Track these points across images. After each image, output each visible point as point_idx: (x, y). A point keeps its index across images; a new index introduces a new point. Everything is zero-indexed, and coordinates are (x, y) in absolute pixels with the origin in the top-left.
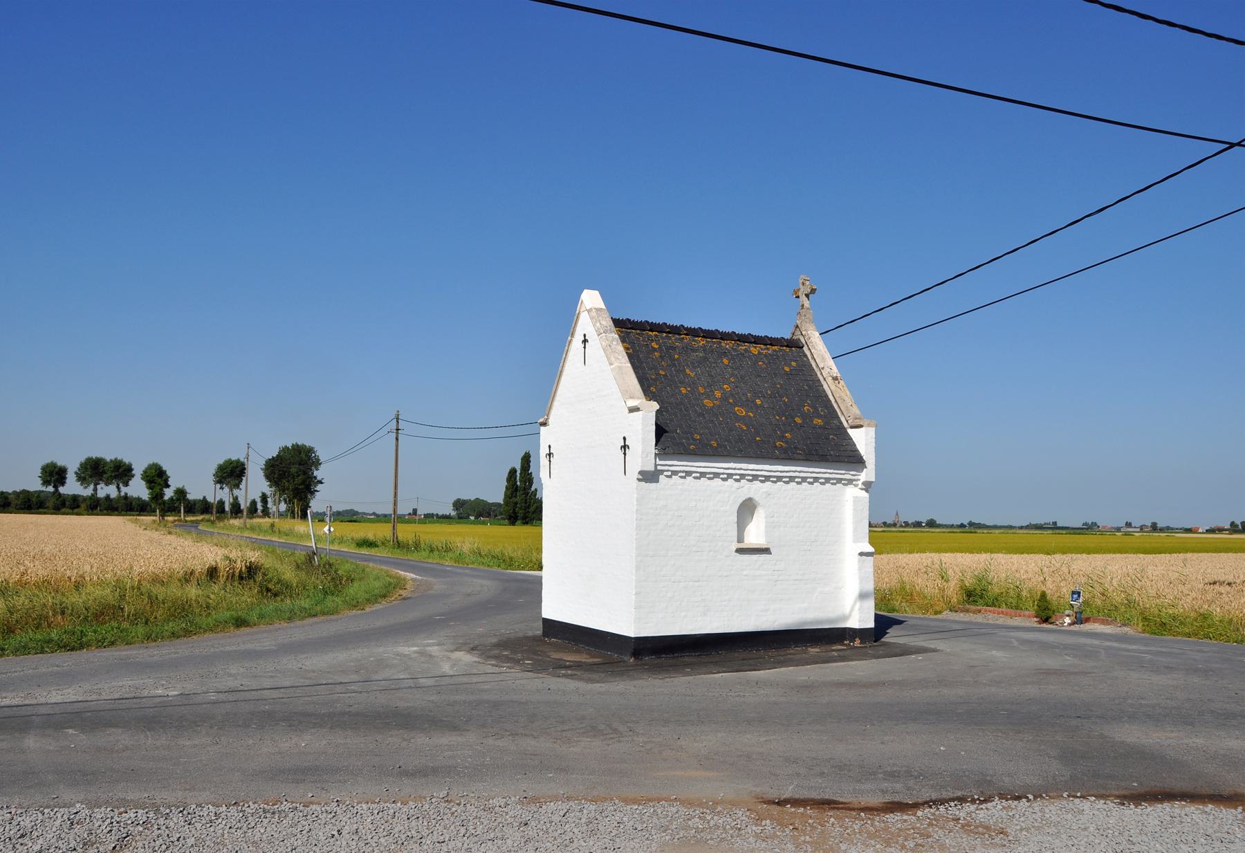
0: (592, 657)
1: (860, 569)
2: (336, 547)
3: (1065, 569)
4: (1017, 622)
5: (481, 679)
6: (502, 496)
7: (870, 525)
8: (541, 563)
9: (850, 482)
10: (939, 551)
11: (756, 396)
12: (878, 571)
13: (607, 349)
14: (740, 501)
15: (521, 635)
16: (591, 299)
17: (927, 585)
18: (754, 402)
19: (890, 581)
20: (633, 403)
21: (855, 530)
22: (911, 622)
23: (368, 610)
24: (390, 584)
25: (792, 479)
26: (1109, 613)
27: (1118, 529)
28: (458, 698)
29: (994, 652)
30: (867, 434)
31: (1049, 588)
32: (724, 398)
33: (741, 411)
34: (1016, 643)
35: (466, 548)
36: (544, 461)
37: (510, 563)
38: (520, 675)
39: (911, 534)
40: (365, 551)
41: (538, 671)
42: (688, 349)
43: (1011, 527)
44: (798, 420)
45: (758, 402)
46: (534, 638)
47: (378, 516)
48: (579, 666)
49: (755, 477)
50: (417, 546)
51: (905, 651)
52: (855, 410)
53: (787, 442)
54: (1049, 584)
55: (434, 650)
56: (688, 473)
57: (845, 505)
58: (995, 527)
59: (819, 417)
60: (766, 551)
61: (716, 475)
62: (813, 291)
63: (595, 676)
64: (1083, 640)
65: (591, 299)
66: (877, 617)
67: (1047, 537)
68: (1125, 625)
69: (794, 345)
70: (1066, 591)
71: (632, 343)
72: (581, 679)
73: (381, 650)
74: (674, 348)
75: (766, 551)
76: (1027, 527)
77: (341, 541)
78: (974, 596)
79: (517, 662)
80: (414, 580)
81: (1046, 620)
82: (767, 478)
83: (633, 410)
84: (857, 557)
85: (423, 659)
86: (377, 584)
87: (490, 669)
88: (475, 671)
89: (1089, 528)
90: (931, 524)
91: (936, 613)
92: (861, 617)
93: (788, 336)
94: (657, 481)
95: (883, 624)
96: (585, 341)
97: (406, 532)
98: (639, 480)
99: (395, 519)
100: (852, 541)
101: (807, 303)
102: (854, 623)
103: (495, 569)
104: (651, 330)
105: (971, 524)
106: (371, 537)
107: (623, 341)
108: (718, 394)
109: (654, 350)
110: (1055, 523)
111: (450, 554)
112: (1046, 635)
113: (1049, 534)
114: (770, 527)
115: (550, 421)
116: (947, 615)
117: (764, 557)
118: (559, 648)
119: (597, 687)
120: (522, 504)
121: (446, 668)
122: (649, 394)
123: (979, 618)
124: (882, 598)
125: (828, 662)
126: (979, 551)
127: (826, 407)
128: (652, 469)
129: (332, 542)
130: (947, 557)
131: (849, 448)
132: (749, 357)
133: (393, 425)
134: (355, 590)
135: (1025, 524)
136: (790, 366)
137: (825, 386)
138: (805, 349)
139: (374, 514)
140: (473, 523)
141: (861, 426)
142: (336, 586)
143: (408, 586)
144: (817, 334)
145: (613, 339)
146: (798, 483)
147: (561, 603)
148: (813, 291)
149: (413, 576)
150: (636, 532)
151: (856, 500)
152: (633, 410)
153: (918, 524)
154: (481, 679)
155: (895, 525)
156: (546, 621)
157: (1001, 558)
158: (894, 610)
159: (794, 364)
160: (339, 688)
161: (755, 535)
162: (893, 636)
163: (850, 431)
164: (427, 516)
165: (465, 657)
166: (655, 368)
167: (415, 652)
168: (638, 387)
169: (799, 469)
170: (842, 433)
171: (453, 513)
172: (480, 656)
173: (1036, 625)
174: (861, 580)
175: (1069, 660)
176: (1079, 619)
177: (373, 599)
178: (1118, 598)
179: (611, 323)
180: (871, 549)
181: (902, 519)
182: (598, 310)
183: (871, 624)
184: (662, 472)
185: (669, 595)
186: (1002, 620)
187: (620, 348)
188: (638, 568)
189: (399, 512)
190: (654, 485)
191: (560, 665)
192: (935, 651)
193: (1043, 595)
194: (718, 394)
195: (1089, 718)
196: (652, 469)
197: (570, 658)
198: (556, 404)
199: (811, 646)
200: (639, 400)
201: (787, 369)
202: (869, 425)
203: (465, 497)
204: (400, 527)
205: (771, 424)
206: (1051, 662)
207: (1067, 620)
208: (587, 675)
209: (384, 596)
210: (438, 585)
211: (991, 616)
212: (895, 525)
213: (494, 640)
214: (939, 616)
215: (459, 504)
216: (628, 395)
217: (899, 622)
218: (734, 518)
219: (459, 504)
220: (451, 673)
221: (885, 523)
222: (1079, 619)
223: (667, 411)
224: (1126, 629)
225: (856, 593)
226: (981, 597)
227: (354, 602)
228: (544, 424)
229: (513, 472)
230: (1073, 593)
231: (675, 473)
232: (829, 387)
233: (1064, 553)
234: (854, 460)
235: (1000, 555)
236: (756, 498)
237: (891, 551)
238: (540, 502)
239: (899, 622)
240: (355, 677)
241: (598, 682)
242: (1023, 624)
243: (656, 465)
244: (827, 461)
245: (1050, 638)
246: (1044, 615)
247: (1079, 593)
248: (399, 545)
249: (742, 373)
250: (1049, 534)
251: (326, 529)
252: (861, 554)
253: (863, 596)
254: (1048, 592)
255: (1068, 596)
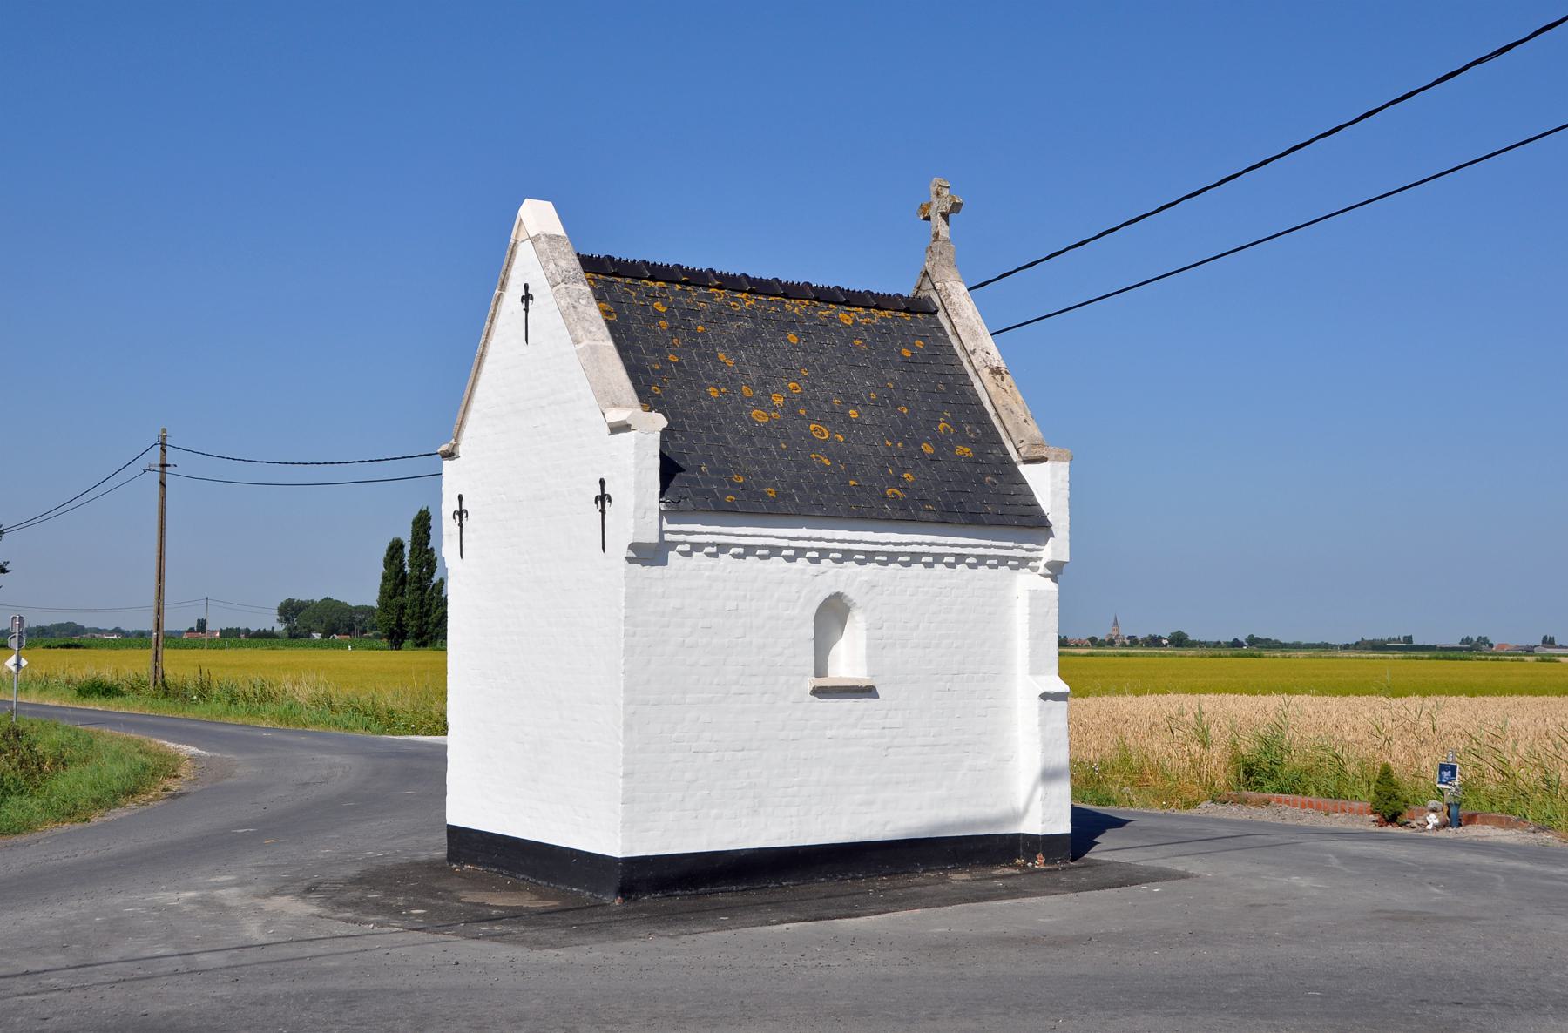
0: (544, 898)
1: (1042, 724)
2: (33, 698)
3: (1425, 722)
4: (1338, 821)
5: (323, 948)
6: (377, 595)
7: (1063, 643)
8: (443, 715)
9: (1023, 563)
10: (1192, 690)
11: (849, 402)
12: (1077, 728)
13: (569, 314)
14: (820, 599)
15: (404, 859)
16: (538, 217)
17: (1169, 753)
18: (845, 414)
19: (1101, 748)
20: (616, 416)
21: (1033, 653)
22: (1140, 823)
23: (96, 820)
24: (145, 767)
25: (915, 558)
26: (1512, 806)
27: (1529, 650)
28: (274, 988)
29: (1295, 879)
30: (1054, 476)
31: (1397, 759)
32: (790, 407)
33: (819, 431)
34: (1335, 862)
35: (303, 693)
36: (448, 526)
37: (390, 721)
38: (400, 937)
39: (1144, 659)
40: (95, 704)
41: (436, 929)
42: (722, 315)
43: (1326, 646)
44: (927, 449)
45: (853, 414)
46: (432, 866)
47: (126, 634)
48: (515, 915)
49: (847, 555)
50: (204, 691)
51: (1127, 878)
52: (1033, 430)
53: (905, 489)
54: (1397, 749)
55: (231, 896)
56: (723, 548)
57: (1015, 604)
58: (1297, 646)
59: (966, 442)
60: (868, 691)
61: (775, 551)
62: (956, 207)
63: (546, 935)
64: (1462, 857)
65: (538, 217)
66: (1076, 814)
67: (1392, 666)
68: (1544, 829)
69: (921, 308)
70: (1429, 765)
71: (616, 302)
72: (521, 942)
73: (119, 900)
74: (695, 313)
75: (868, 691)
76: (1357, 646)
77: (45, 685)
78: (1257, 773)
79: (396, 912)
80: (192, 757)
81: (1393, 819)
82: (870, 557)
83: (617, 428)
84: (1037, 702)
85: (206, 914)
86: (118, 769)
87: (341, 928)
88: (311, 934)
89: (1474, 648)
90: (1179, 640)
91: (1188, 805)
92: (1048, 815)
93: (908, 291)
94: (664, 563)
95: (1089, 825)
96: (527, 298)
97: (180, 666)
98: (629, 560)
99: (159, 640)
100: (1030, 673)
101: (944, 231)
102: (1034, 825)
103: (360, 733)
104: (652, 279)
105: (1253, 641)
106: (107, 675)
107: (600, 298)
108: (778, 399)
109: (659, 315)
110: (1409, 639)
111: (269, 706)
112: (1393, 846)
113: (1400, 660)
114: (876, 647)
115: (461, 449)
116: (1206, 809)
117: (864, 703)
118: (478, 883)
119: (550, 955)
120: (412, 608)
121: (253, 930)
122: (648, 400)
123: (1265, 815)
124: (1085, 777)
125: (985, 899)
126: (1268, 690)
127: (979, 424)
128: (655, 539)
129: (24, 687)
130: (1209, 701)
131: (1021, 499)
132: (837, 331)
133: (155, 457)
134: (66, 783)
135: (1352, 641)
136: (912, 347)
137: (978, 386)
138: (941, 315)
139: (117, 631)
140: (316, 645)
141: (1043, 460)
142: (29, 776)
143: (182, 771)
144: (963, 288)
145: (580, 295)
146: (951, 565)
147: (486, 792)
148: (956, 207)
149: (194, 750)
150: (612, 663)
151: (1034, 595)
152: (617, 428)
153: (1155, 641)
154: (323, 948)
155: (1111, 643)
156: (454, 832)
157: (1306, 704)
158: (1109, 801)
159: (919, 343)
160: (20, 985)
161: (846, 664)
162: (1106, 849)
163: (1024, 469)
164: (226, 633)
165: (293, 907)
166: (659, 350)
167: (191, 901)
168: (627, 385)
169: (942, 539)
170: (1007, 470)
171: (280, 628)
172: (322, 903)
173: (1373, 828)
174: (1046, 745)
175: (1436, 895)
176: (1455, 818)
177: (108, 799)
178: (1529, 777)
179: (576, 264)
180: (1063, 687)
181: (1126, 632)
182: (552, 238)
183: (1065, 827)
184: (673, 545)
185: (688, 776)
186: (1310, 819)
187: (594, 311)
188: (628, 727)
189: (168, 626)
190: (656, 570)
191: (478, 916)
192: (1184, 876)
193: (1386, 772)
194: (778, 399)
195: (1477, 1005)
196: (655, 539)
197: (499, 900)
198: (472, 417)
199: (955, 869)
200: (629, 410)
201: (907, 353)
202: (1057, 458)
203: (302, 596)
204: (168, 655)
205: (876, 454)
206: (1400, 897)
207: (1433, 819)
208: (531, 933)
209: (133, 792)
210: (244, 767)
211: (1288, 811)
212: (1111, 643)
213: (352, 871)
214: (1193, 812)
215: (290, 610)
216: (607, 400)
217: (1118, 823)
218: (809, 631)
219: (290, 610)
220: (263, 939)
221: (1093, 641)
222: (1455, 818)
223: (683, 431)
224: (1546, 837)
225: (1037, 769)
226: (1272, 775)
227: (68, 807)
228: (450, 455)
229: (396, 548)
230: (1442, 768)
231: (697, 547)
232: (984, 387)
233: (1425, 694)
234: (1034, 523)
235: (1306, 698)
236: (851, 593)
237: (1104, 691)
238: (444, 603)
239: (1118, 823)
240: (59, 959)
241: (553, 946)
242: (1349, 826)
243: (661, 533)
244: (981, 523)
245: (1401, 852)
246: (1388, 810)
247: (1453, 769)
248: (166, 690)
249: (824, 360)
250: (1400, 660)
251: (11, 663)
252: (1045, 696)
253: (1048, 776)
254: (1395, 766)
255: (1433, 773)
